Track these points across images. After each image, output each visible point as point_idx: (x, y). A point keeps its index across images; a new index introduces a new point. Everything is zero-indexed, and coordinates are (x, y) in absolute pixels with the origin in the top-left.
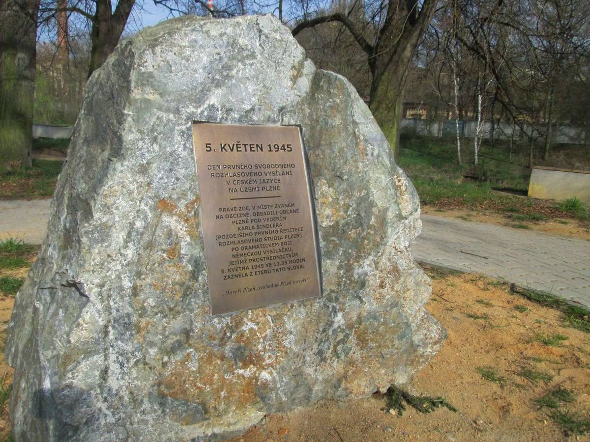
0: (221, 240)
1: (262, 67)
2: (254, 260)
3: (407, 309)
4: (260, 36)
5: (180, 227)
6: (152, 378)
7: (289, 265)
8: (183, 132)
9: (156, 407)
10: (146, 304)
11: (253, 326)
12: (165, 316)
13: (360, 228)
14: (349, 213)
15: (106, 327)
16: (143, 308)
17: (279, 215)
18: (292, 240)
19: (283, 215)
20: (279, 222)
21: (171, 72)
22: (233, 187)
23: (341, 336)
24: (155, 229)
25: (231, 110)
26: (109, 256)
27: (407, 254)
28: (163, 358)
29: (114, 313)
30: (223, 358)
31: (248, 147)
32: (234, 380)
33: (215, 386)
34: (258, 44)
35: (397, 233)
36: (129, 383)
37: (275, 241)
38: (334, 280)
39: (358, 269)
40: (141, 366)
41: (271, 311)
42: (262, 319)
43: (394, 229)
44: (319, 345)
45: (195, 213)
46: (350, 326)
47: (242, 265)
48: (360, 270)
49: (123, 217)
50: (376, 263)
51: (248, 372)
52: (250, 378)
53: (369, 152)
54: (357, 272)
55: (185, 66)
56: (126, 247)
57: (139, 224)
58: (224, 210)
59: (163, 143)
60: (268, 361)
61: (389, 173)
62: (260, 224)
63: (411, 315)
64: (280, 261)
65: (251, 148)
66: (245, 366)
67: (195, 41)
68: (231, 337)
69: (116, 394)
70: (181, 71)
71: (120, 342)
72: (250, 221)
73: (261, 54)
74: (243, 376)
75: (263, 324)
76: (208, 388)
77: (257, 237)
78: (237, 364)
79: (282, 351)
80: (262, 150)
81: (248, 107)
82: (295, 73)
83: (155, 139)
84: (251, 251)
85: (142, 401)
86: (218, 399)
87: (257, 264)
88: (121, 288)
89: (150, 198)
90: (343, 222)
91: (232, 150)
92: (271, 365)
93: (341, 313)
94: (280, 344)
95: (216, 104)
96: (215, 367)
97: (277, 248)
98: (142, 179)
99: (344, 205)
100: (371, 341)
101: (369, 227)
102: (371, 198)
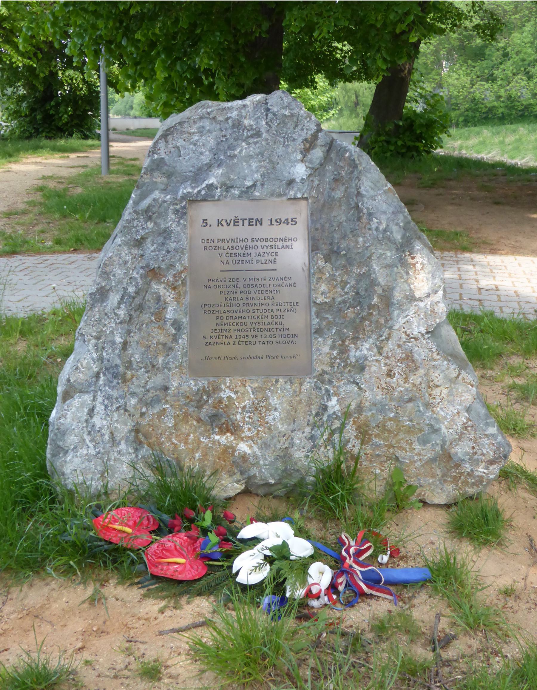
0: (207, 308)
1: (268, 144)
2: (239, 330)
3: (438, 409)
4: (267, 115)
5: (168, 294)
6: (130, 424)
7: (277, 338)
8: (178, 211)
9: (131, 450)
10: (132, 359)
11: (231, 395)
12: (147, 372)
13: (359, 308)
14: (346, 290)
15: (98, 373)
16: (130, 362)
17: (272, 288)
18: (283, 314)
19: (277, 288)
20: (271, 295)
21: (180, 156)
22: (224, 258)
23: (337, 424)
24: (145, 295)
25: (232, 187)
26: (106, 314)
27: (425, 342)
28: (141, 408)
29: (106, 362)
30: (199, 420)
31: (246, 222)
32: (210, 445)
33: (190, 446)
34: (264, 123)
35: (406, 316)
36: (111, 424)
37: (264, 314)
38: (327, 359)
39: (356, 352)
40: (122, 411)
41: (252, 383)
42: (241, 389)
43: (403, 311)
44: (312, 429)
45: (182, 283)
46: (347, 414)
47: (225, 334)
48: (358, 353)
49: (118, 282)
50: (380, 349)
51: (224, 439)
52: (226, 448)
53: (374, 226)
54: (353, 354)
55: (192, 150)
56: (119, 308)
57: (131, 290)
58: (213, 280)
59: (159, 221)
60: (248, 434)
61: (397, 249)
62: (249, 296)
63: (445, 418)
64: (268, 334)
65: (249, 222)
66: (222, 432)
67: (203, 127)
68: (207, 401)
69: (99, 431)
70: (189, 154)
71: (107, 388)
72: (238, 292)
73: (268, 131)
74: (219, 442)
75: (242, 394)
76: (182, 447)
77: (245, 308)
78: (213, 430)
79: (265, 427)
80: (261, 224)
81: (249, 183)
82: (308, 145)
83: (150, 218)
84: (236, 321)
85: (120, 442)
86: (192, 460)
87: (242, 334)
88: (113, 343)
89: (142, 268)
90: (339, 299)
91: (229, 225)
92: (251, 438)
93: (336, 398)
94: (262, 418)
95: (216, 183)
96: (191, 427)
97: (266, 321)
98: (136, 252)
99: (342, 281)
100: (376, 436)
101: (371, 307)
102: (373, 276)
